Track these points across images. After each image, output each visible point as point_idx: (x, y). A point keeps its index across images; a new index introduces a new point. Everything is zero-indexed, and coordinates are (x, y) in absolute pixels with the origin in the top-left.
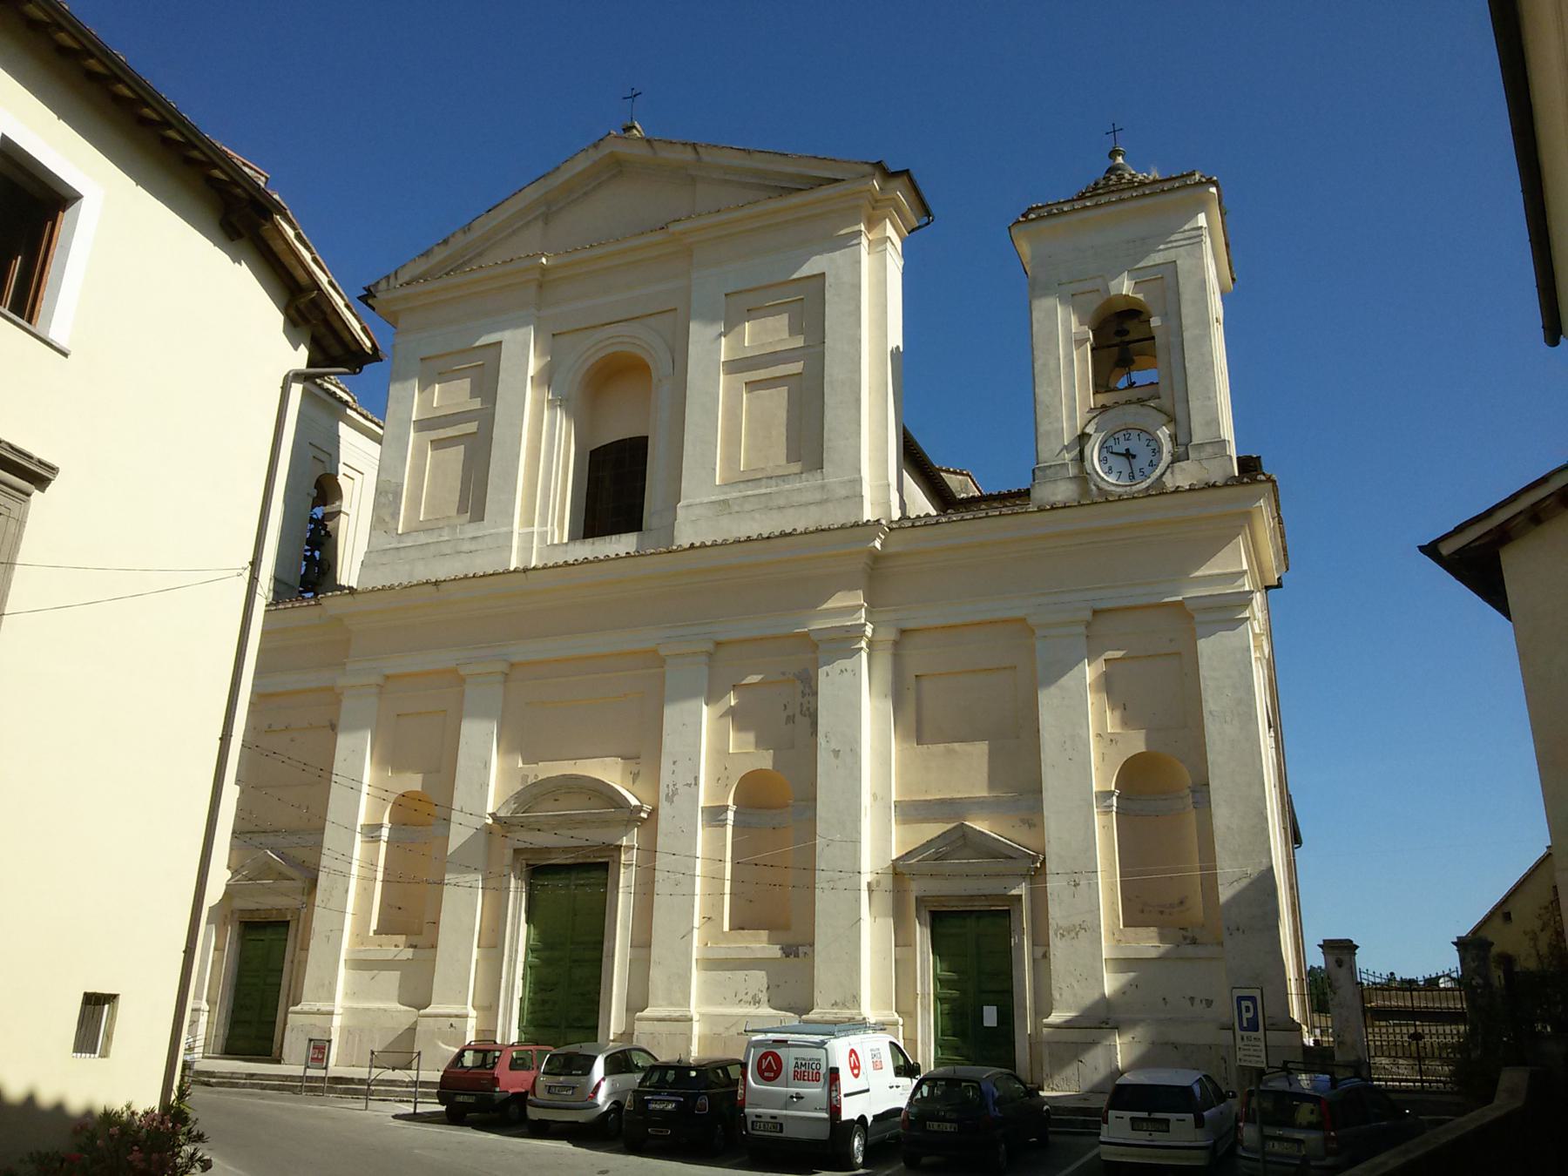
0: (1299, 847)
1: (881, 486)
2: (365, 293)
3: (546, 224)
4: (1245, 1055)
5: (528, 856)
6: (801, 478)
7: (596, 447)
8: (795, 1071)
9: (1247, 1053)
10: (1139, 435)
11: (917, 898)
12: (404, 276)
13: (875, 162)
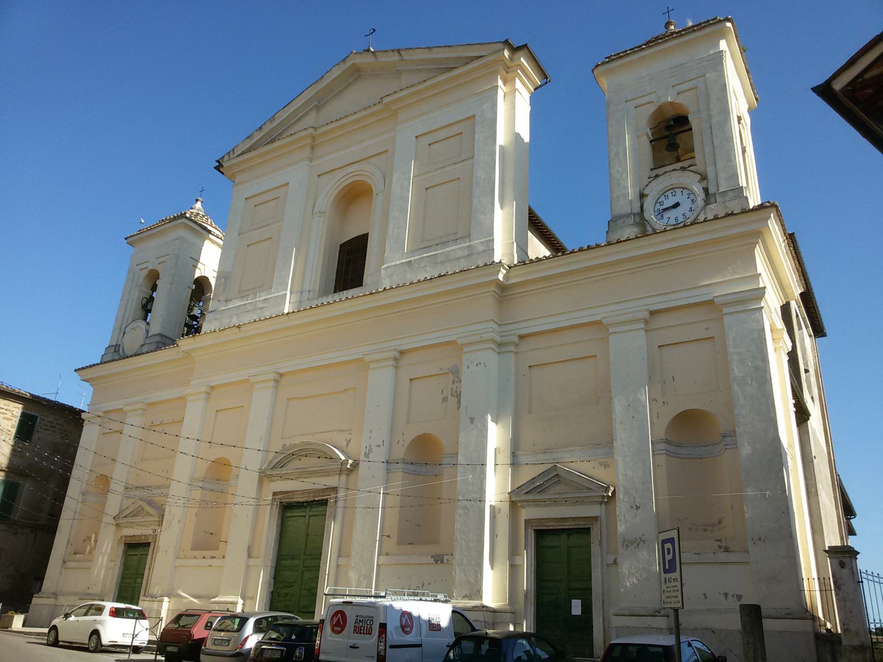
0: (855, 517)
1: (509, 243)
2: (218, 164)
3: (318, 112)
4: (667, 598)
6: (456, 243)
7: (343, 242)
8: (355, 626)
9: (668, 594)
10: (682, 192)
11: (525, 520)
13: (504, 41)
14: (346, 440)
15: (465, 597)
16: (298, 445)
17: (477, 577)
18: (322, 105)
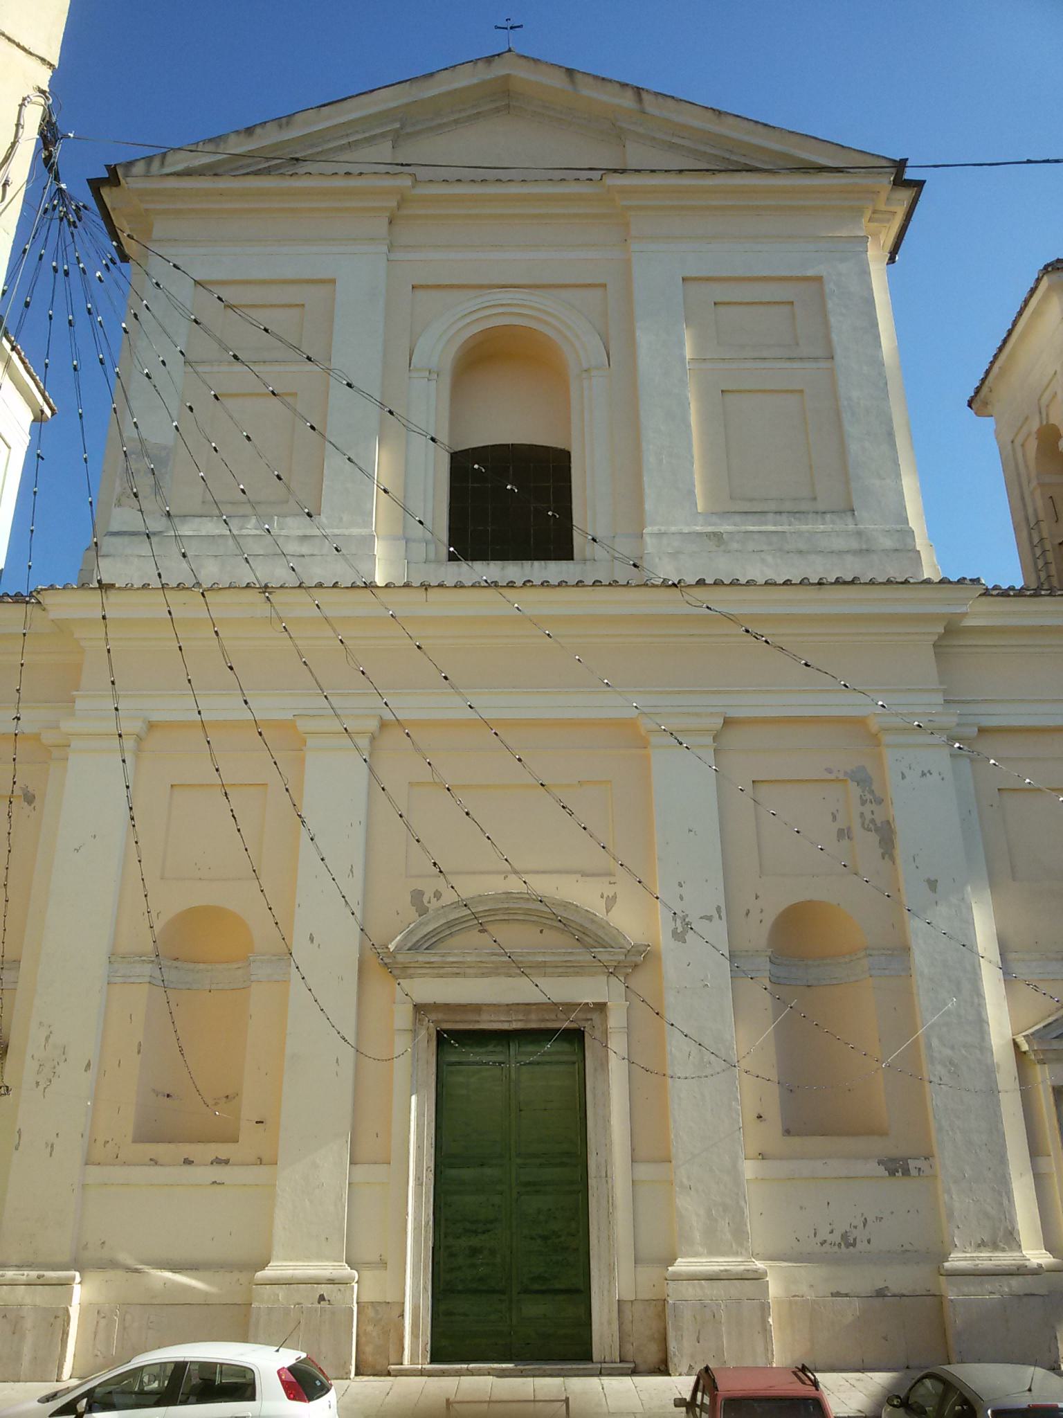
5: (440, 1016)
6: (824, 519)
12: (179, 162)
14: (602, 897)
15: (981, 1245)
16: (493, 898)
17: (1001, 1204)
18: (408, 134)
